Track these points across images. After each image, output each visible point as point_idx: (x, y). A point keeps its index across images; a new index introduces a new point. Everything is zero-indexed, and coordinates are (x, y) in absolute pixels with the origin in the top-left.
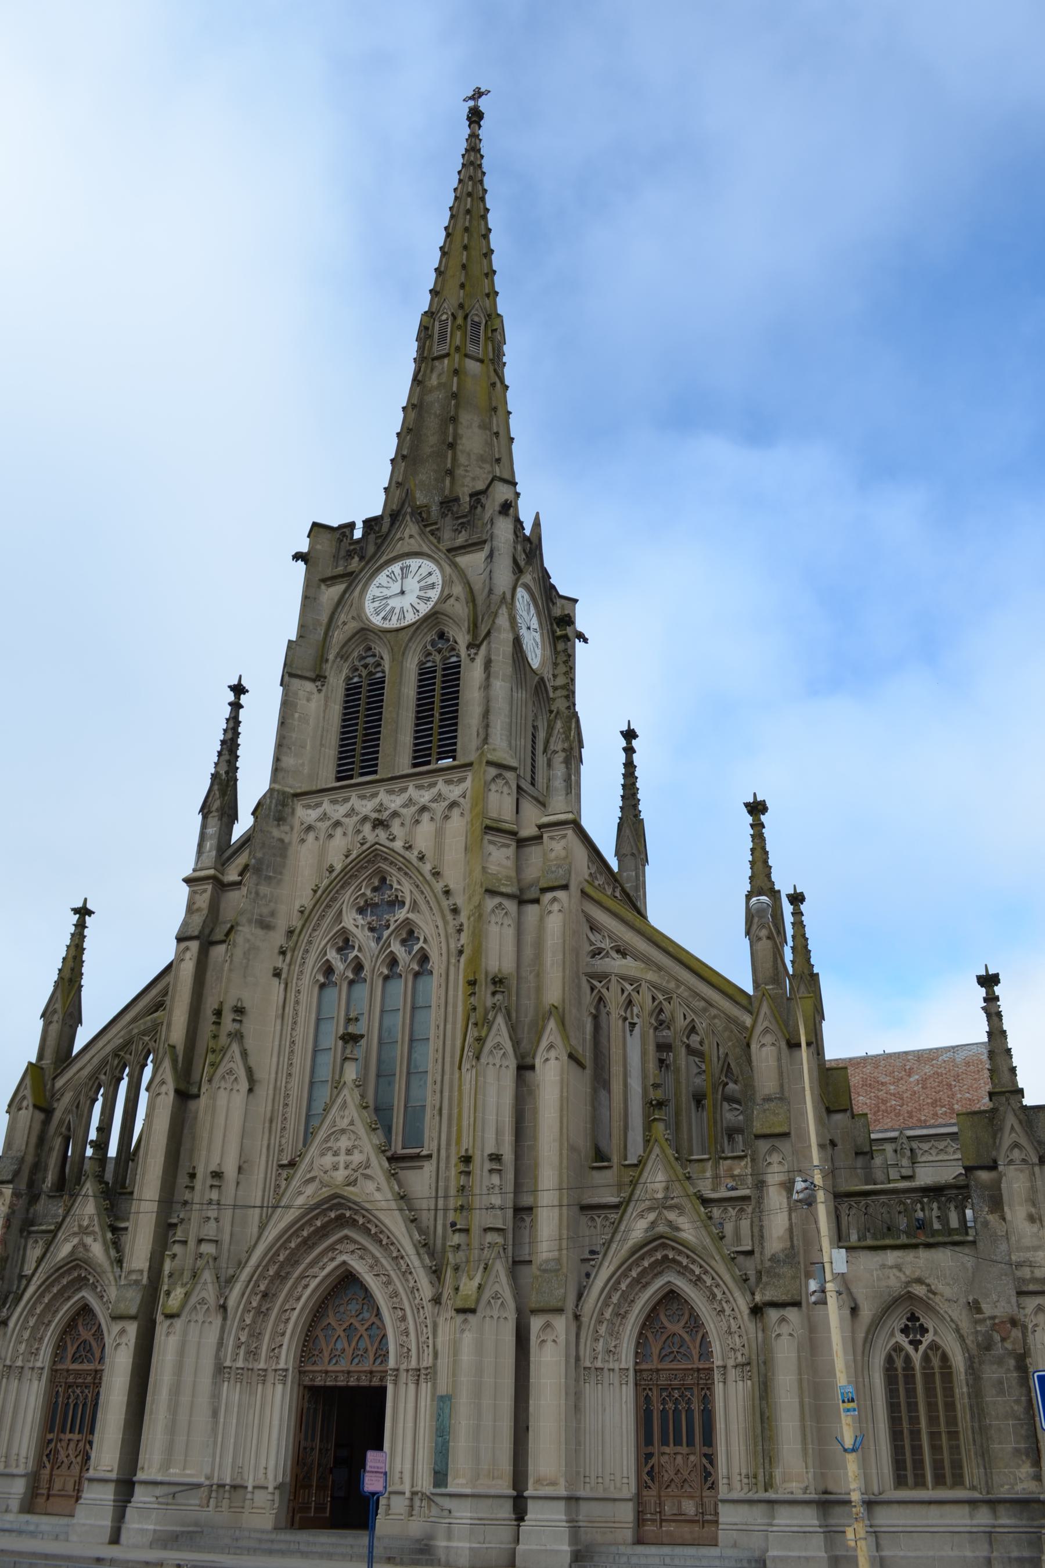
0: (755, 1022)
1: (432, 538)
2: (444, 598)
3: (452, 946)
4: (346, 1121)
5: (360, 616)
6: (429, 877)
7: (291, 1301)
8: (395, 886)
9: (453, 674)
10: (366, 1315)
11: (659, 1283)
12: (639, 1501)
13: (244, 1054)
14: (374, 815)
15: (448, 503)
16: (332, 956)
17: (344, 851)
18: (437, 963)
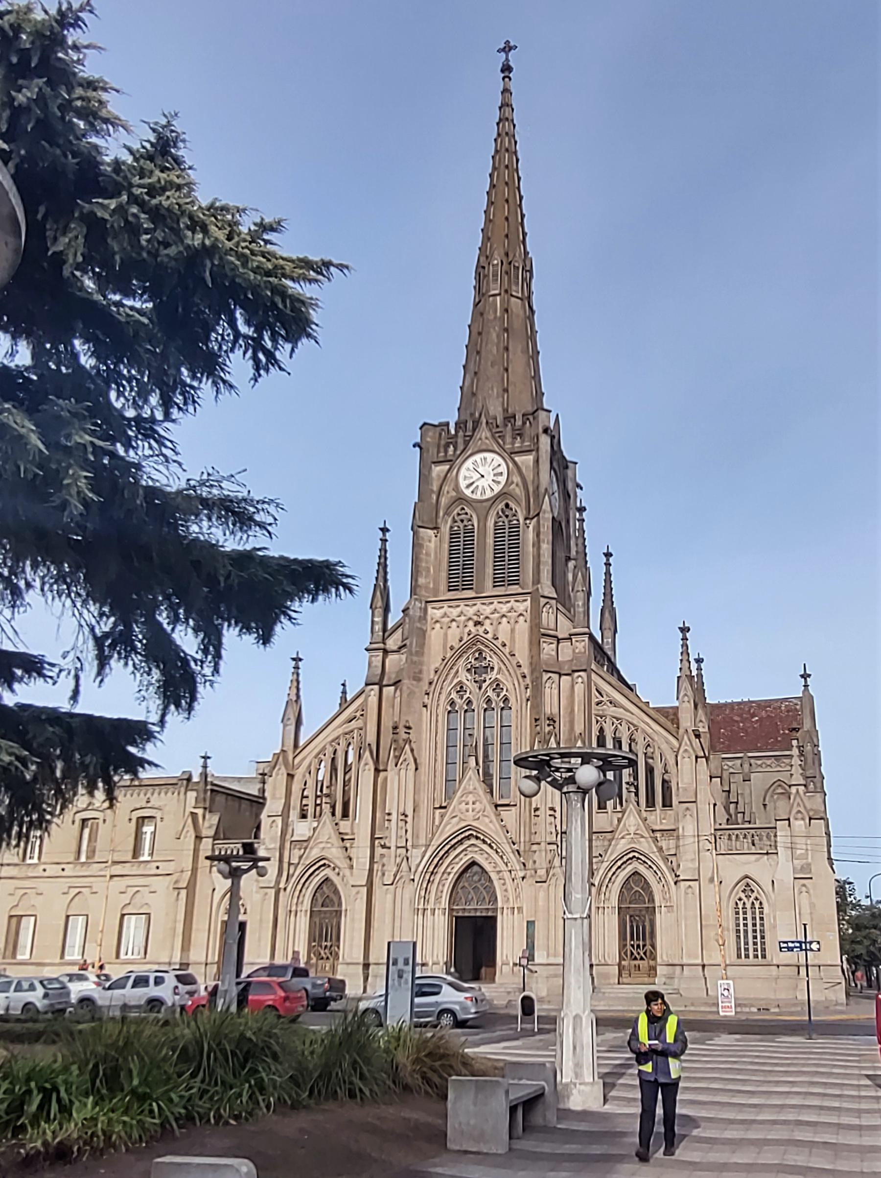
0: (680, 745)
1: (500, 441)
2: (508, 482)
3: (523, 697)
4: (471, 787)
5: (457, 488)
6: (509, 657)
7: (445, 875)
8: (488, 658)
9: (515, 532)
10: (483, 881)
11: (630, 868)
12: (619, 965)
13: (412, 750)
14: (475, 618)
15: (510, 418)
16: (454, 695)
17: (458, 638)
18: (512, 702)
